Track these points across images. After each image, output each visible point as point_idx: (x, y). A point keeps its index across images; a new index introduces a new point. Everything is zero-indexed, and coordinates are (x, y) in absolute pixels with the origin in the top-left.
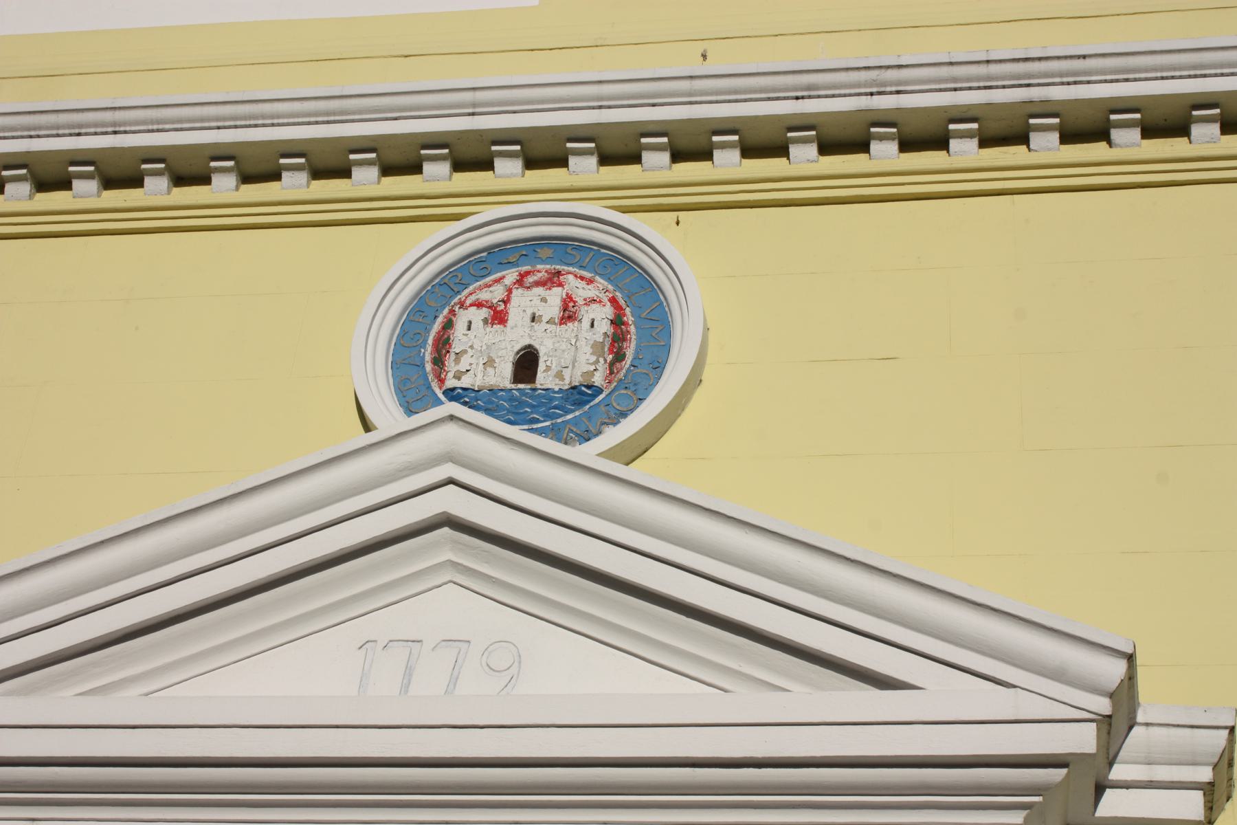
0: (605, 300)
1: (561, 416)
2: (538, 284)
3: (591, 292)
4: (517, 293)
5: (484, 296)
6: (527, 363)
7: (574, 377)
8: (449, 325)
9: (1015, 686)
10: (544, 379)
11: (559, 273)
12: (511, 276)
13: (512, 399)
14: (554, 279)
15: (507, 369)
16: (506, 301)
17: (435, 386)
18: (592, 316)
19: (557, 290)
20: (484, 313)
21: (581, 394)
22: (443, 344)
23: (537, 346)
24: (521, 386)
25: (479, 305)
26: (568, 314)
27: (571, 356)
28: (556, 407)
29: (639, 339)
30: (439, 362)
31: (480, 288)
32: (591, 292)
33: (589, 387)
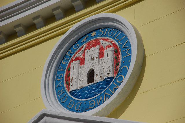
0: (112, 45)
1: (104, 90)
2: (92, 46)
3: (108, 43)
4: (87, 51)
5: (78, 55)
6: (91, 75)
7: (105, 76)
8: (69, 70)
9: (131, 24)
10: (97, 79)
11: (98, 40)
12: (85, 46)
13: (89, 89)
14: (97, 43)
15: (86, 79)
16: (84, 55)
17: (67, 91)
18: (107, 53)
19: (98, 47)
20: (78, 61)
21: (108, 81)
22: (68, 75)
23: (93, 69)
24: (90, 84)
25: (76, 60)
26: (101, 55)
27: (104, 68)
28: (101, 88)
29: (123, 66)
30: (68, 84)
31: (76, 53)
32: (108, 43)
33: (108, 78)
